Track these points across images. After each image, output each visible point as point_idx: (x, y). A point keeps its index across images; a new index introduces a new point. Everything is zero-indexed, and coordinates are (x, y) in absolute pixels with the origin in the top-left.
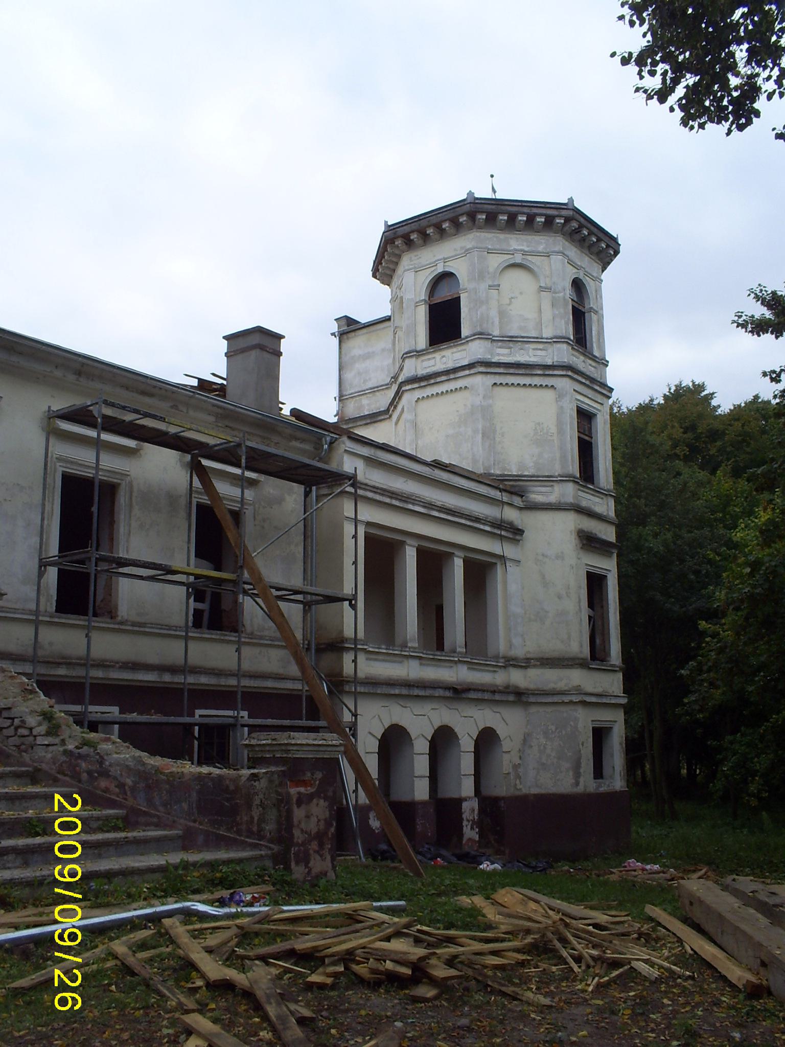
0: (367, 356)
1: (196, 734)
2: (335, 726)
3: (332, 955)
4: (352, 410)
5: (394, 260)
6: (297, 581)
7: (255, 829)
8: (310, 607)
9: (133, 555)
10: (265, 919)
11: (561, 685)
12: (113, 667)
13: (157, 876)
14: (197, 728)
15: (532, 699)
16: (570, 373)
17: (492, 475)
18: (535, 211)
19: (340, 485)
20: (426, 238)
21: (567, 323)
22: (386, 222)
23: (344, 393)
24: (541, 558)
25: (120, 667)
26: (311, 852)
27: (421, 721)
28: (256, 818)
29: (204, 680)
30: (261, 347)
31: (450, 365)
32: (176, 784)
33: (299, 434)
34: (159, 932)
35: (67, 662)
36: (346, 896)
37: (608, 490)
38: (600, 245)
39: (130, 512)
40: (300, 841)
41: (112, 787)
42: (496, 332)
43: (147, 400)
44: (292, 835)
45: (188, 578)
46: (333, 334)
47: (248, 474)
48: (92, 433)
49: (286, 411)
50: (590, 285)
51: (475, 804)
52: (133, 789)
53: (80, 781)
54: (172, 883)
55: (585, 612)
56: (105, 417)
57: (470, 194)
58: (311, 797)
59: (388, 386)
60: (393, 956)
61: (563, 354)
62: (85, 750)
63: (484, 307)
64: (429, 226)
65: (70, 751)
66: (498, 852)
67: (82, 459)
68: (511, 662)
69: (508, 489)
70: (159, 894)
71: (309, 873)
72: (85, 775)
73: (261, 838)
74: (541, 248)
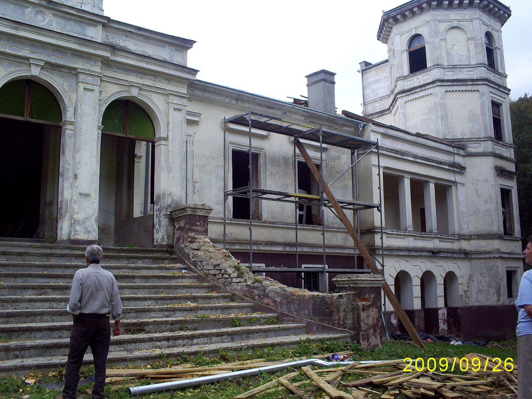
0: (378, 81)
1: (303, 276)
2: (375, 271)
3: (392, 385)
4: (370, 110)
5: (389, 30)
6: (349, 198)
7: (342, 323)
8: (357, 211)
9: (268, 188)
10: (353, 367)
11: (489, 249)
12: (261, 244)
13: (295, 346)
14: (303, 273)
15: (473, 256)
16: (487, 83)
17: (448, 139)
19: (370, 148)
20: (405, 17)
21: (484, 56)
22: (383, 11)
23: (366, 101)
24: (475, 182)
25: (265, 244)
26: (370, 334)
27: (416, 269)
28: (342, 318)
29: (305, 249)
30: (325, 80)
31: (422, 83)
32: (301, 300)
33: (347, 123)
34: (301, 373)
35: (240, 242)
36: (389, 356)
37: (510, 144)
39: (266, 167)
40: (364, 329)
41: (270, 302)
43: (271, 111)
44: (360, 327)
45: (295, 199)
46: (358, 71)
47: (324, 145)
48: (246, 129)
49: (339, 112)
50: (495, 34)
51: (445, 311)
52: (281, 303)
53: (254, 300)
54: (303, 349)
55: (501, 209)
56: (252, 120)
58: (369, 307)
59: (388, 96)
60: (423, 386)
61: (483, 73)
62: (256, 284)
63: (438, 51)
64: (406, 11)
66: (457, 336)
67: (243, 143)
68: (462, 237)
69: (456, 146)
70: (297, 355)
71: (369, 345)
72: (257, 296)
73: (345, 327)
74: (467, 17)
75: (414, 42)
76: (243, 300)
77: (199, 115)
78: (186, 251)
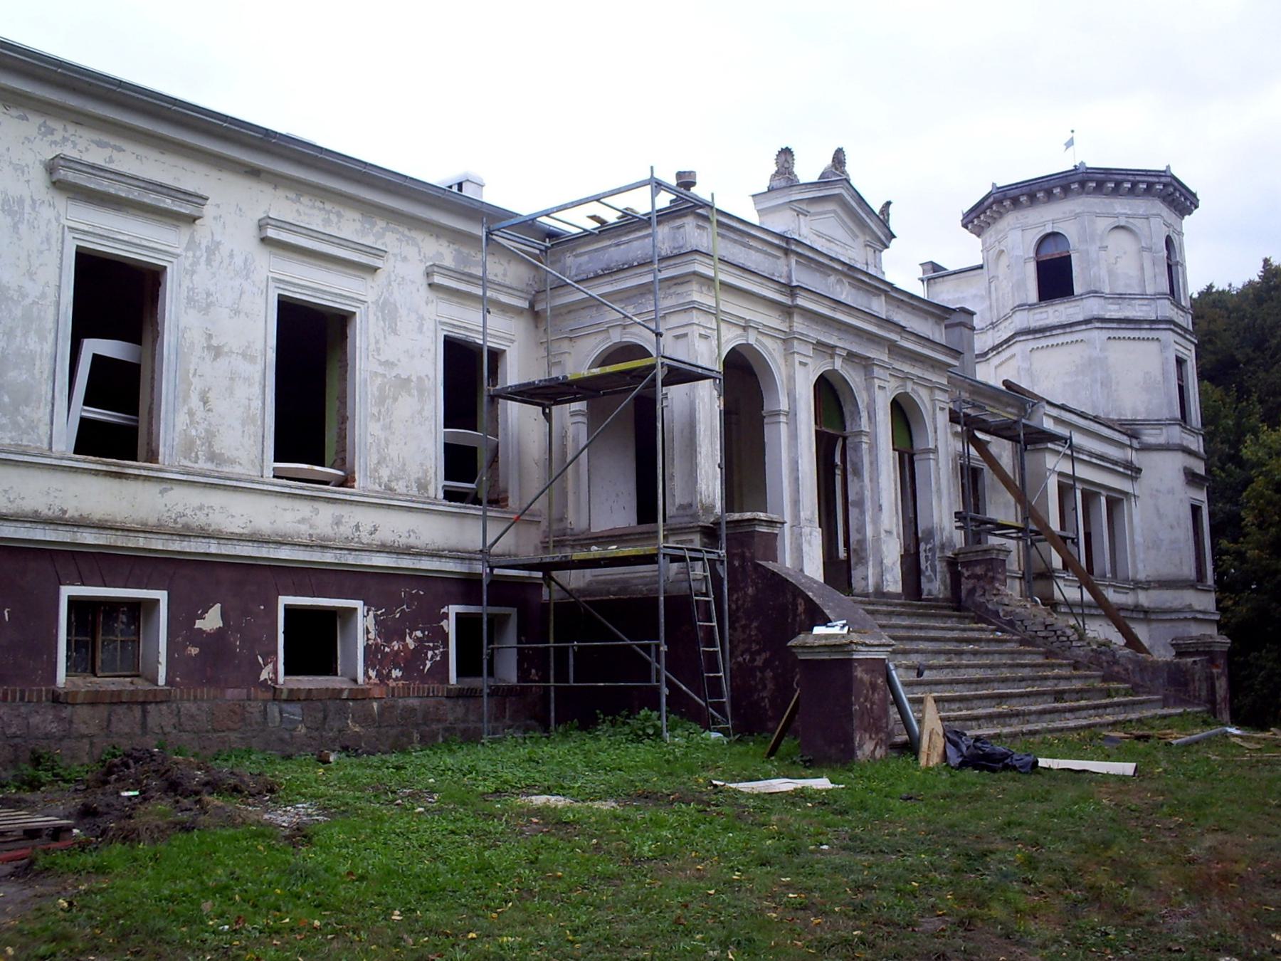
11: (1176, 604)
18: (1138, 178)
31: (1065, 320)
38: (1179, 198)
42: (1107, 291)
50: (1175, 237)
52: (1133, 671)
56: (966, 415)
57: (1082, 163)
76: (1089, 668)
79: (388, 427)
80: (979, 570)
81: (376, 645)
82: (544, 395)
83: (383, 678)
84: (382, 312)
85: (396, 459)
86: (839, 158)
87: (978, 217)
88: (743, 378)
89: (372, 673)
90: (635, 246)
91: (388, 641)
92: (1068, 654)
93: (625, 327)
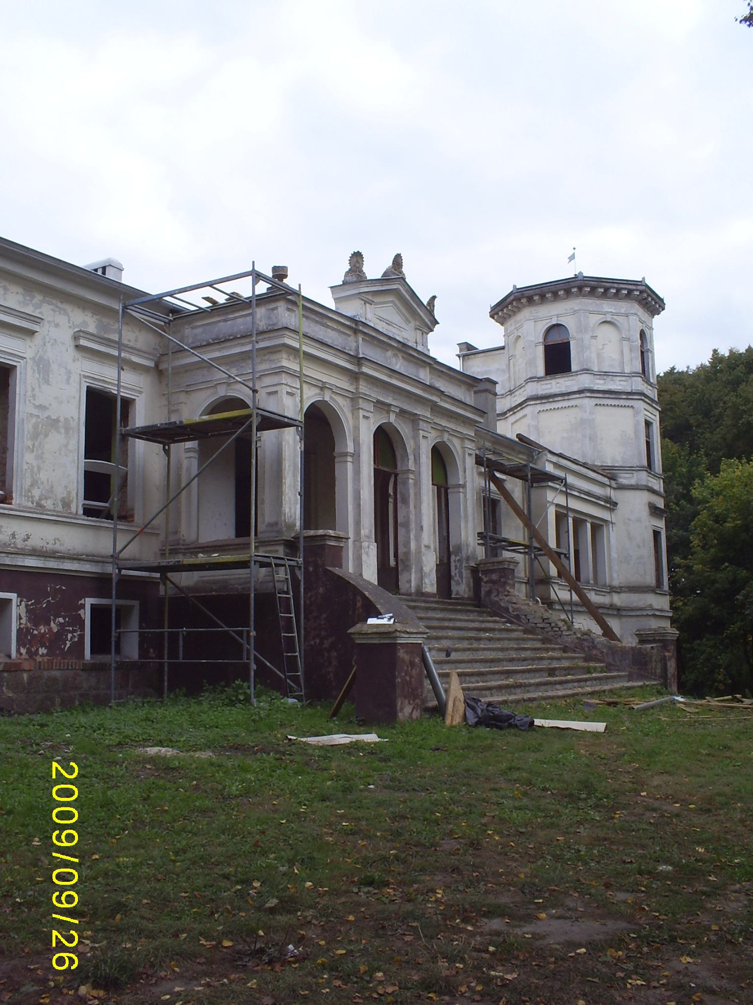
11: (641, 604)
31: (564, 390)
38: (651, 302)
42: (596, 370)
50: (647, 331)
65: (632, 649)
74: (623, 311)
75: (552, 331)
76: (575, 652)
77: (37, 320)
78: (502, 604)
79: (40, 457)
80: (494, 577)
81: (27, 628)
82: (165, 435)
83: (32, 655)
84: (38, 366)
85: (45, 482)
86: (398, 261)
87: (502, 310)
88: (319, 426)
89: (23, 651)
90: (239, 322)
91: (36, 625)
92: (559, 640)
93: (229, 384)
